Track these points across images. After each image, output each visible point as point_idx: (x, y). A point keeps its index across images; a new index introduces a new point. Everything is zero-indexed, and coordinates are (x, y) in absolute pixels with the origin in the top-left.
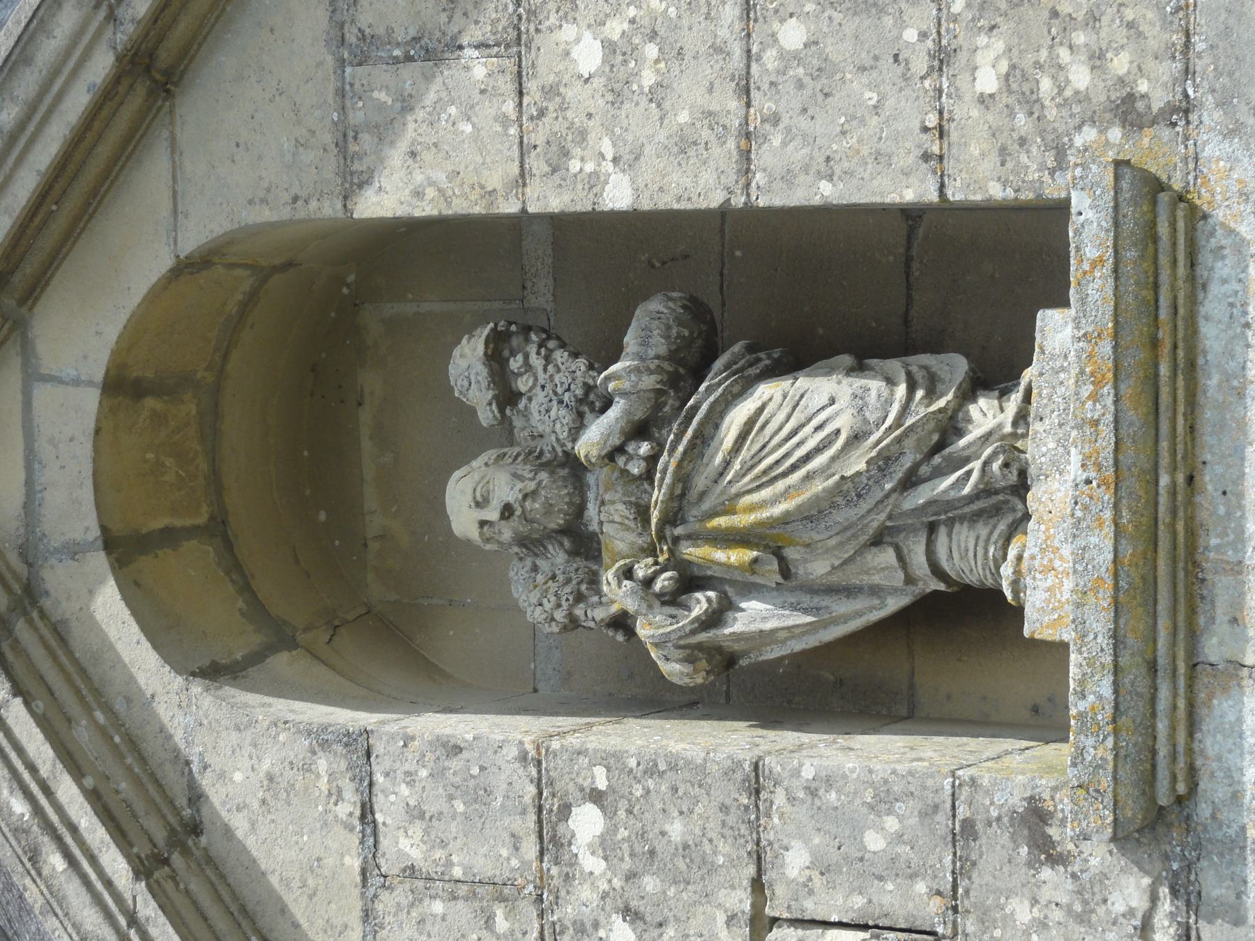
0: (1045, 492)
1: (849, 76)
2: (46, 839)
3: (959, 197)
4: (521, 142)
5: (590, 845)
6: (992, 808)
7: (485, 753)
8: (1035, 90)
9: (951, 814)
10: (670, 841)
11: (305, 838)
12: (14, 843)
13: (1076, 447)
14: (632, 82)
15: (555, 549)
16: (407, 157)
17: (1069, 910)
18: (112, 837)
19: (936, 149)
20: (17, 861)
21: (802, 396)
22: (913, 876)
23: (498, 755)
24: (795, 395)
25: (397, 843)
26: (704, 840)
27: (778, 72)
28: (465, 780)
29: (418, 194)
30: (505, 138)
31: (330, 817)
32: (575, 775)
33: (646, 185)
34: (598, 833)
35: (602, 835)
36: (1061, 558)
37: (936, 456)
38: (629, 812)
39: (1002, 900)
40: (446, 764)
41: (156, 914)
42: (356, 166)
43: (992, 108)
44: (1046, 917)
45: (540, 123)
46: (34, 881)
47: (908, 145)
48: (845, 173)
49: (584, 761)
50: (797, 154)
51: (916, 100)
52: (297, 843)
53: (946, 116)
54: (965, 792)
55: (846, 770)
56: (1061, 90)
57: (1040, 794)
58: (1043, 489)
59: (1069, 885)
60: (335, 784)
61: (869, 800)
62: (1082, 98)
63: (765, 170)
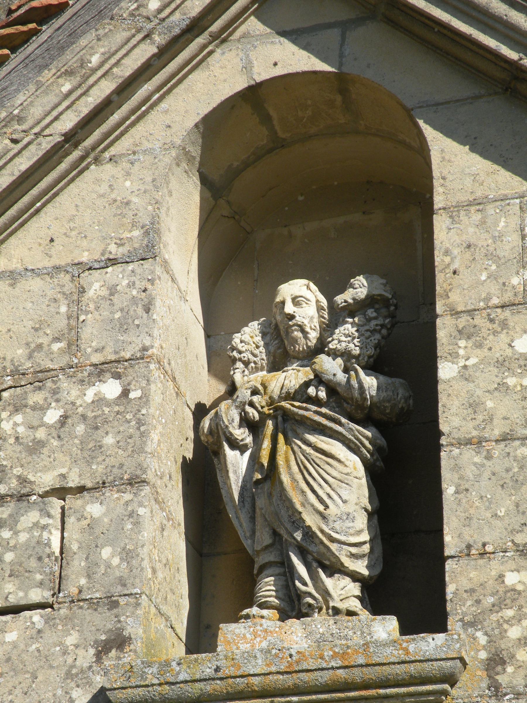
0: (296, 629)
1: (513, 498)
2: (78, 79)
3: (447, 567)
4: (475, 310)
5: (99, 392)
6: (124, 617)
7: (147, 327)
8: (507, 607)
9: (122, 594)
10: (103, 437)
11: (97, 228)
12: (75, 59)
13: (308, 647)
14: (509, 372)
15: (276, 344)
16: (467, 243)
17: (73, 666)
18: (83, 118)
19: (473, 552)
20: (65, 63)
21: (347, 484)
22: (89, 576)
23: (146, 334)
24: (347, 480)
25: (97, 282)
26: (104, 457)
27: (515, 457)
28: (131, 317)
29: (447, 252)
30: (478, 300)
31: (108, 241)
32: (136, 379)
33: (451, 386)
34: (106, 396)
35: (105, 399)
36: (261, 642)
37: (317, 564)
38: (118, 413)
39: (77, 628)
40: (140, 305)
41: (43, 149)
42: (462, 213)
43: (496, 582)
44: (69, 654)
45: (486, 320)
46: (54, 75)
47: (475, 536)
48: (460, 501)
49: (144, 383)
50: (470, 472)
51: (500, 538)
52: (94, 223)
53: (492, 556)
54: (132, 600)
55: (143, 533)
56: (507, 622)
57: (133, 643)
58: (298, 627)
59: (86, 665)
60: (126, 241)
61: (128, 547)
62: (503, 633)
63: (461, 454)
